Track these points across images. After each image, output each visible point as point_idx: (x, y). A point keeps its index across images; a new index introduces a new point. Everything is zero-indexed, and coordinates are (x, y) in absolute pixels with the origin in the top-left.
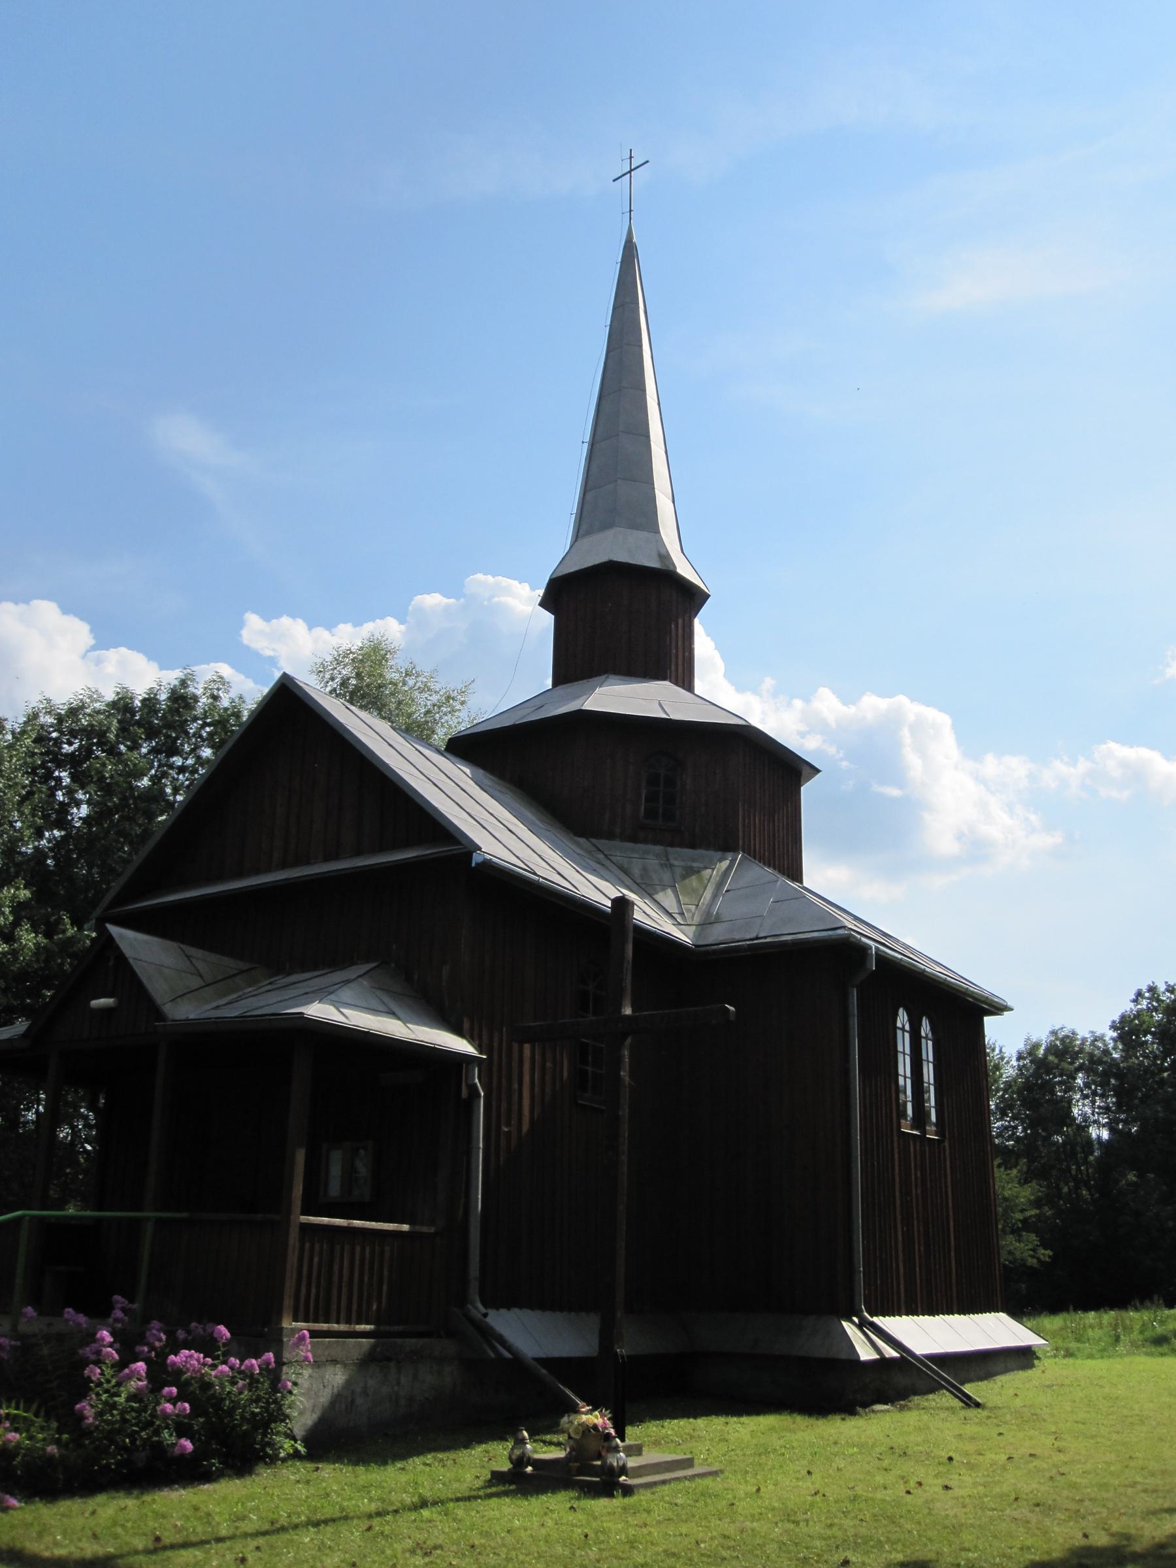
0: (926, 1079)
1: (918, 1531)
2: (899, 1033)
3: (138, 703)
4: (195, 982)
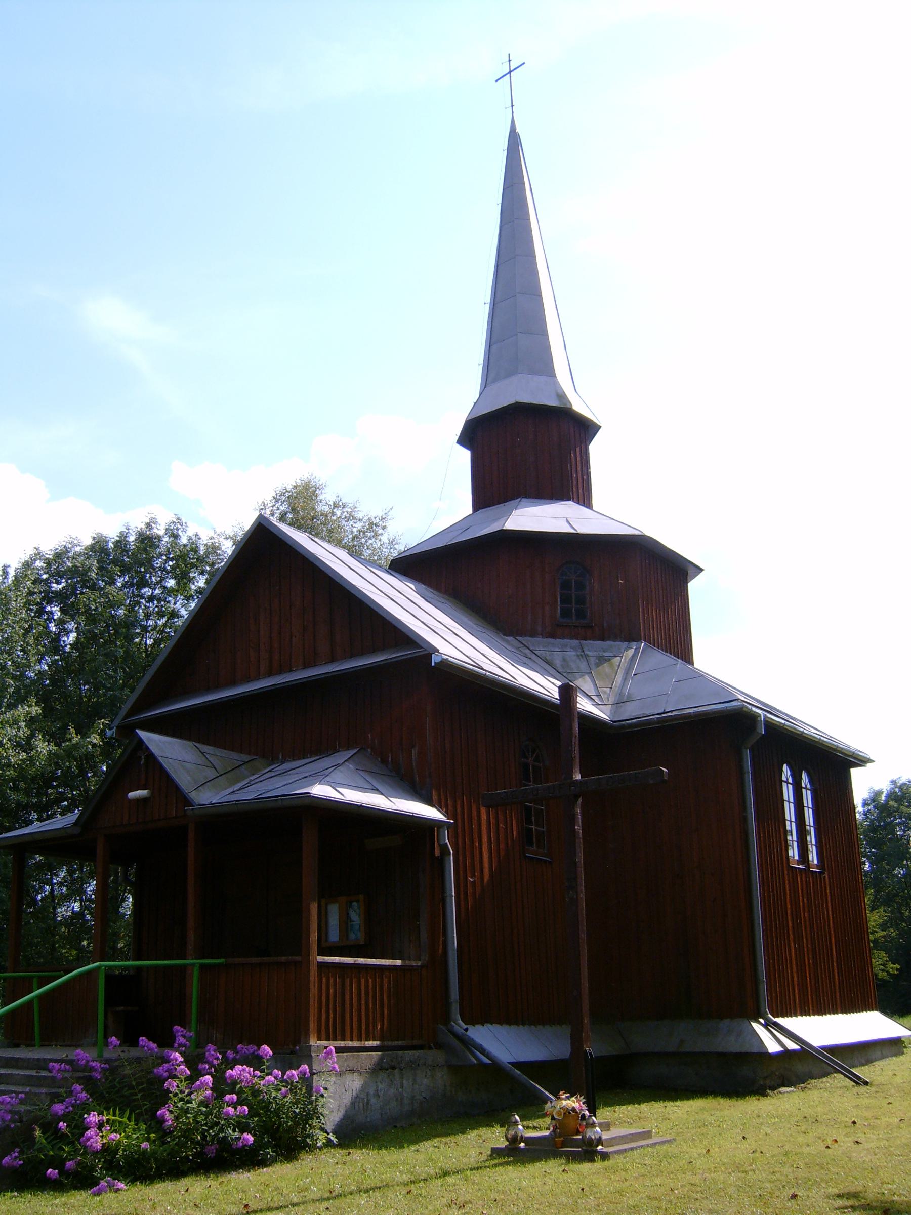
0: (807, 823)
1: (844, 1173)
2: (784, 785)
3: (111, 545)
4: (211, 773)
